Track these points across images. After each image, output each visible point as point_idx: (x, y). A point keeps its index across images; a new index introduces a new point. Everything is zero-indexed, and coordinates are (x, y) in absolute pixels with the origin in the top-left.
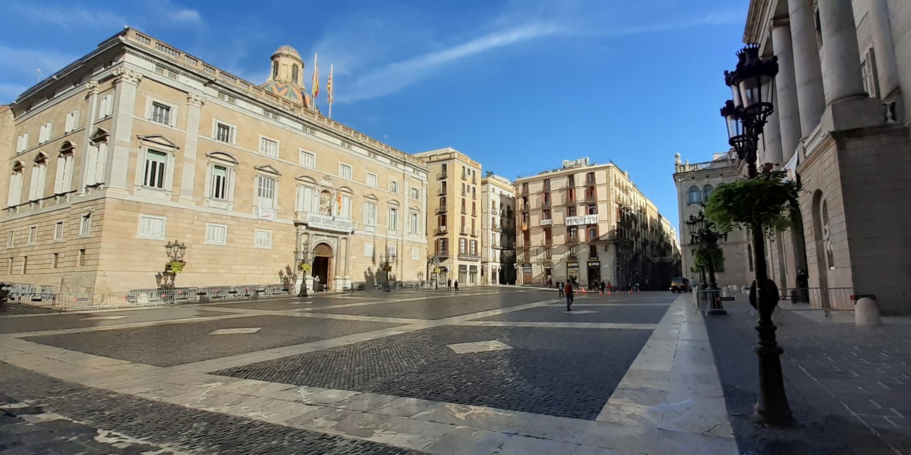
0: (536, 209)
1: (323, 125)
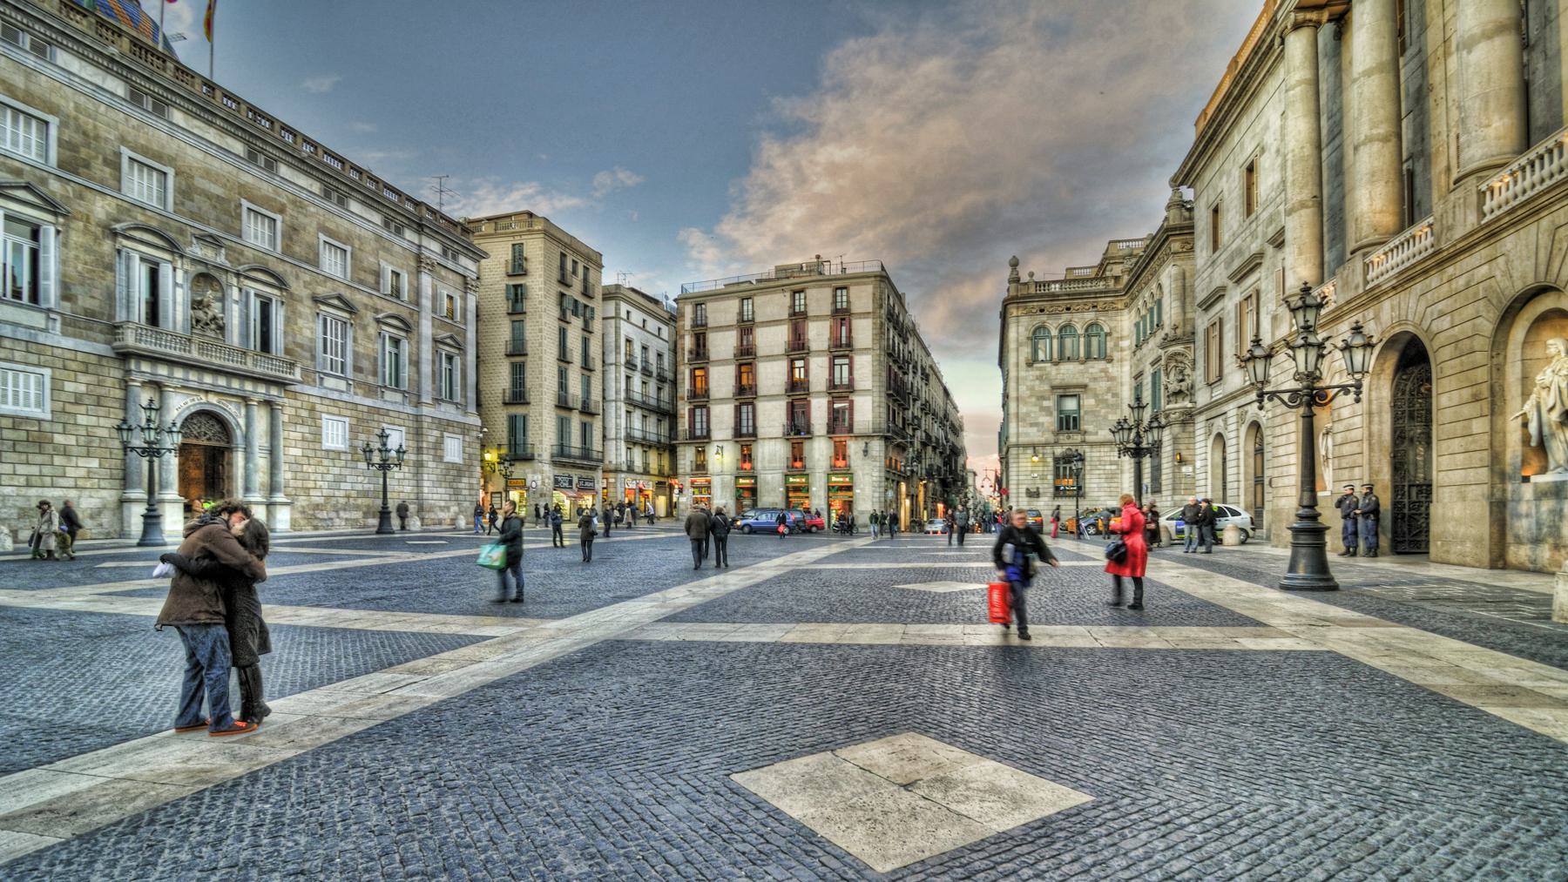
0: (1370, 140)
1: (191, 93)
